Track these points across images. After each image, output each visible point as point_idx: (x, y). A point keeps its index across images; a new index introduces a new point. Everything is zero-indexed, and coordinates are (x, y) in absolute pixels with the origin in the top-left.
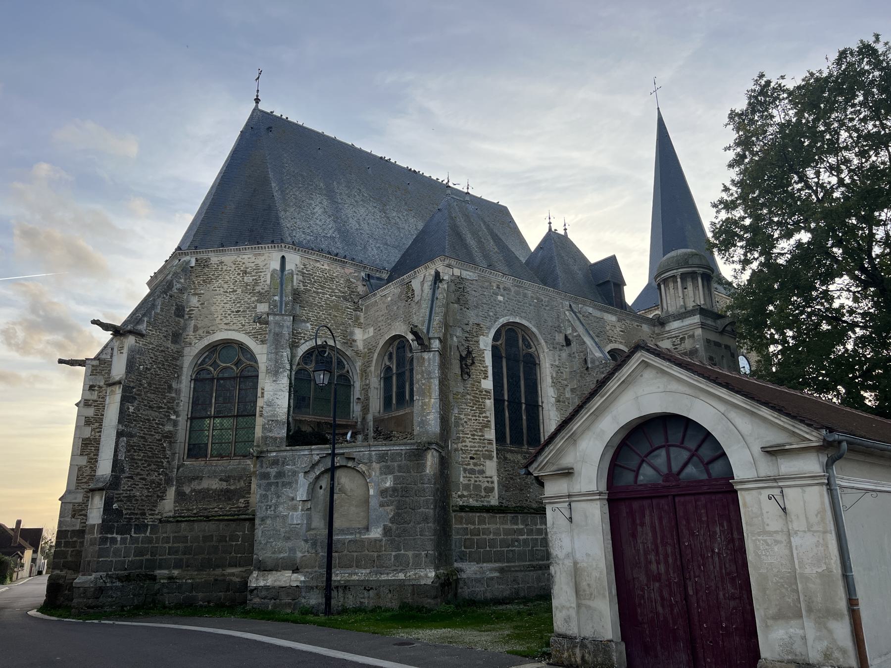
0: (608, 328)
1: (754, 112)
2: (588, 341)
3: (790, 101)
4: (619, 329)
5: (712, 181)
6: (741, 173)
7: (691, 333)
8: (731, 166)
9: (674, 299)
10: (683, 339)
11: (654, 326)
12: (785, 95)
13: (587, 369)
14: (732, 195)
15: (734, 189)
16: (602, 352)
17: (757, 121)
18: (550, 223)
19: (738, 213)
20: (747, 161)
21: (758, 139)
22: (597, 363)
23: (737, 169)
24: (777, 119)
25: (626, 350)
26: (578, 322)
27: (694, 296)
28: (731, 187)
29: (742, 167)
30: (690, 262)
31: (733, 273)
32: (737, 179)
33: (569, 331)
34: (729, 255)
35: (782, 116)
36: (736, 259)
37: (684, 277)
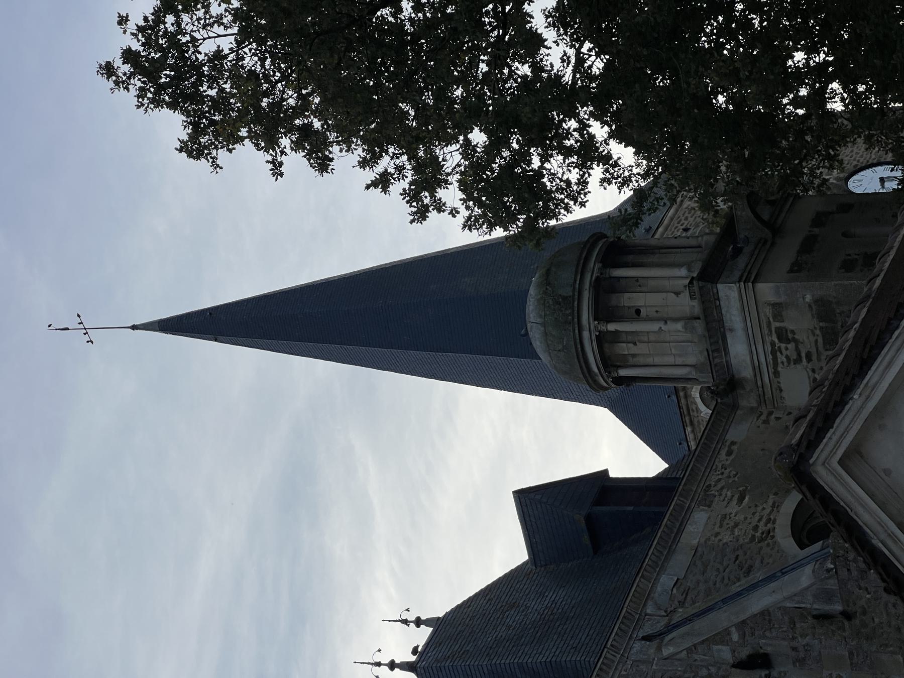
0: (726, 538)
1: (197, 97)
2: (759, 602)
3: (186, 10)
4: (733, 508)
5: (351, 217)
6: (348, 143)
7: (768, 311)
8: (323, 165)
9: (663, 341)
10: (783, 335)
11: (735, 407)
12: (170, 19)
13: (847, 616)
14: (400, 169)
15: (385, 163)
16: (799, 565)
17: (222, 90)
18: (392, 665)
19: (451, 157)
20: (317, 124)
21: (266, 94)
22: (832, 584)
23: (335, 149)
24: (227, 44)
25: (793, 500)
26: (700, 625)
27: (661, 294)
28: (380, 169)
29: (332, 136)
30: (567, 291)
31: (613, 187)
32: (359, 152)
33: (725, 653)
34: (560, 190)
35: (220, 30)
36: (574, 176)
37: (604, 313)
